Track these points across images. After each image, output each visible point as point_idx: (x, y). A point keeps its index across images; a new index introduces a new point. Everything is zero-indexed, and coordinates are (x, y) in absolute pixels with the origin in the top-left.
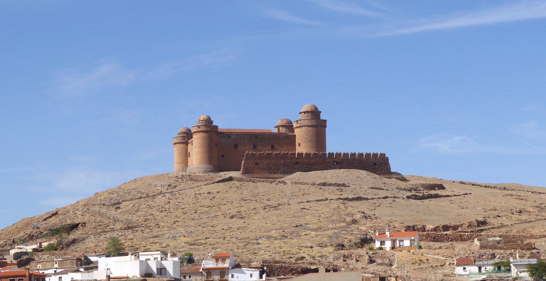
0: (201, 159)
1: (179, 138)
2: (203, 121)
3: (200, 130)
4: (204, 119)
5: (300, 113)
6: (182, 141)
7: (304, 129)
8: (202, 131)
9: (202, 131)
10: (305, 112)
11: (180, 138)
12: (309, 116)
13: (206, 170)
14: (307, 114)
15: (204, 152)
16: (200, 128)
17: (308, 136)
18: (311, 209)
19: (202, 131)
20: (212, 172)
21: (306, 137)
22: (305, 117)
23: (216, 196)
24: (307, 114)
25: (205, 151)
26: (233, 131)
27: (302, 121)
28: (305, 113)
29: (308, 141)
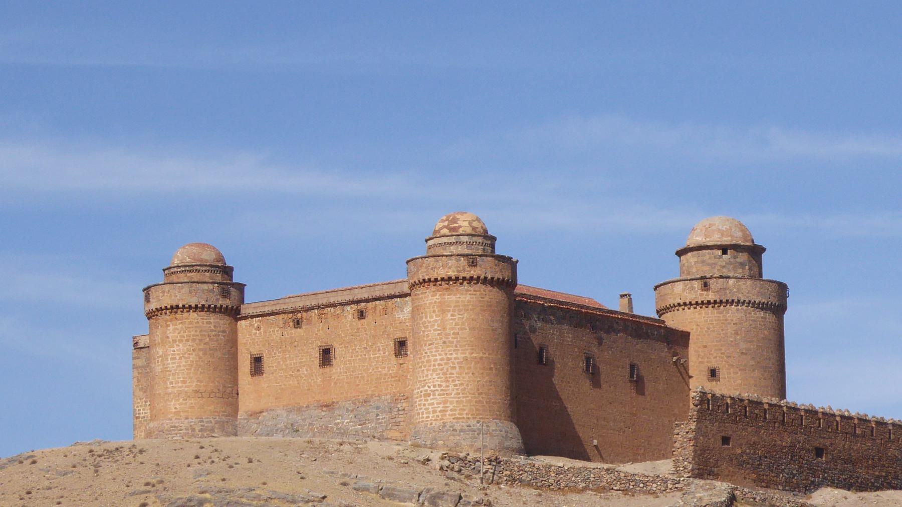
0: (480, 394)
1: (205, 286)
2: (475, 239)
3: (474, 272)
4: (474, 229)
5: (680, 253)
6: (218, 300)
7: (738, 315)
8: (486, 278)
9: (485, 281)
10: (724, 249)
11: (211, 286)
12: (742, 265)
13: (507, 444)
14: (735, 257)
15: (491, 369)
16: (476, 266)
17: (751, 342)
18: (238, 497)
19: (485, 281)
20: (520, 452)
21: (743, 345)
22: (724, 267)
23: (260, 486)
24: (735, 257)
25: (495, 364)
26: (530, 297)
27: (731, 282)
28: (725, 252)
29: (752, 363)
